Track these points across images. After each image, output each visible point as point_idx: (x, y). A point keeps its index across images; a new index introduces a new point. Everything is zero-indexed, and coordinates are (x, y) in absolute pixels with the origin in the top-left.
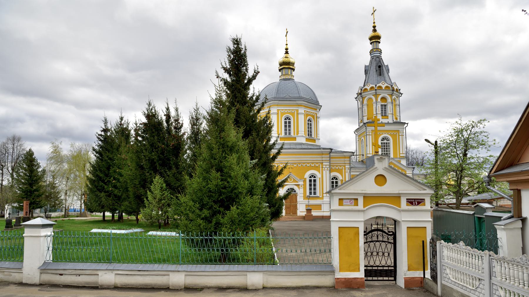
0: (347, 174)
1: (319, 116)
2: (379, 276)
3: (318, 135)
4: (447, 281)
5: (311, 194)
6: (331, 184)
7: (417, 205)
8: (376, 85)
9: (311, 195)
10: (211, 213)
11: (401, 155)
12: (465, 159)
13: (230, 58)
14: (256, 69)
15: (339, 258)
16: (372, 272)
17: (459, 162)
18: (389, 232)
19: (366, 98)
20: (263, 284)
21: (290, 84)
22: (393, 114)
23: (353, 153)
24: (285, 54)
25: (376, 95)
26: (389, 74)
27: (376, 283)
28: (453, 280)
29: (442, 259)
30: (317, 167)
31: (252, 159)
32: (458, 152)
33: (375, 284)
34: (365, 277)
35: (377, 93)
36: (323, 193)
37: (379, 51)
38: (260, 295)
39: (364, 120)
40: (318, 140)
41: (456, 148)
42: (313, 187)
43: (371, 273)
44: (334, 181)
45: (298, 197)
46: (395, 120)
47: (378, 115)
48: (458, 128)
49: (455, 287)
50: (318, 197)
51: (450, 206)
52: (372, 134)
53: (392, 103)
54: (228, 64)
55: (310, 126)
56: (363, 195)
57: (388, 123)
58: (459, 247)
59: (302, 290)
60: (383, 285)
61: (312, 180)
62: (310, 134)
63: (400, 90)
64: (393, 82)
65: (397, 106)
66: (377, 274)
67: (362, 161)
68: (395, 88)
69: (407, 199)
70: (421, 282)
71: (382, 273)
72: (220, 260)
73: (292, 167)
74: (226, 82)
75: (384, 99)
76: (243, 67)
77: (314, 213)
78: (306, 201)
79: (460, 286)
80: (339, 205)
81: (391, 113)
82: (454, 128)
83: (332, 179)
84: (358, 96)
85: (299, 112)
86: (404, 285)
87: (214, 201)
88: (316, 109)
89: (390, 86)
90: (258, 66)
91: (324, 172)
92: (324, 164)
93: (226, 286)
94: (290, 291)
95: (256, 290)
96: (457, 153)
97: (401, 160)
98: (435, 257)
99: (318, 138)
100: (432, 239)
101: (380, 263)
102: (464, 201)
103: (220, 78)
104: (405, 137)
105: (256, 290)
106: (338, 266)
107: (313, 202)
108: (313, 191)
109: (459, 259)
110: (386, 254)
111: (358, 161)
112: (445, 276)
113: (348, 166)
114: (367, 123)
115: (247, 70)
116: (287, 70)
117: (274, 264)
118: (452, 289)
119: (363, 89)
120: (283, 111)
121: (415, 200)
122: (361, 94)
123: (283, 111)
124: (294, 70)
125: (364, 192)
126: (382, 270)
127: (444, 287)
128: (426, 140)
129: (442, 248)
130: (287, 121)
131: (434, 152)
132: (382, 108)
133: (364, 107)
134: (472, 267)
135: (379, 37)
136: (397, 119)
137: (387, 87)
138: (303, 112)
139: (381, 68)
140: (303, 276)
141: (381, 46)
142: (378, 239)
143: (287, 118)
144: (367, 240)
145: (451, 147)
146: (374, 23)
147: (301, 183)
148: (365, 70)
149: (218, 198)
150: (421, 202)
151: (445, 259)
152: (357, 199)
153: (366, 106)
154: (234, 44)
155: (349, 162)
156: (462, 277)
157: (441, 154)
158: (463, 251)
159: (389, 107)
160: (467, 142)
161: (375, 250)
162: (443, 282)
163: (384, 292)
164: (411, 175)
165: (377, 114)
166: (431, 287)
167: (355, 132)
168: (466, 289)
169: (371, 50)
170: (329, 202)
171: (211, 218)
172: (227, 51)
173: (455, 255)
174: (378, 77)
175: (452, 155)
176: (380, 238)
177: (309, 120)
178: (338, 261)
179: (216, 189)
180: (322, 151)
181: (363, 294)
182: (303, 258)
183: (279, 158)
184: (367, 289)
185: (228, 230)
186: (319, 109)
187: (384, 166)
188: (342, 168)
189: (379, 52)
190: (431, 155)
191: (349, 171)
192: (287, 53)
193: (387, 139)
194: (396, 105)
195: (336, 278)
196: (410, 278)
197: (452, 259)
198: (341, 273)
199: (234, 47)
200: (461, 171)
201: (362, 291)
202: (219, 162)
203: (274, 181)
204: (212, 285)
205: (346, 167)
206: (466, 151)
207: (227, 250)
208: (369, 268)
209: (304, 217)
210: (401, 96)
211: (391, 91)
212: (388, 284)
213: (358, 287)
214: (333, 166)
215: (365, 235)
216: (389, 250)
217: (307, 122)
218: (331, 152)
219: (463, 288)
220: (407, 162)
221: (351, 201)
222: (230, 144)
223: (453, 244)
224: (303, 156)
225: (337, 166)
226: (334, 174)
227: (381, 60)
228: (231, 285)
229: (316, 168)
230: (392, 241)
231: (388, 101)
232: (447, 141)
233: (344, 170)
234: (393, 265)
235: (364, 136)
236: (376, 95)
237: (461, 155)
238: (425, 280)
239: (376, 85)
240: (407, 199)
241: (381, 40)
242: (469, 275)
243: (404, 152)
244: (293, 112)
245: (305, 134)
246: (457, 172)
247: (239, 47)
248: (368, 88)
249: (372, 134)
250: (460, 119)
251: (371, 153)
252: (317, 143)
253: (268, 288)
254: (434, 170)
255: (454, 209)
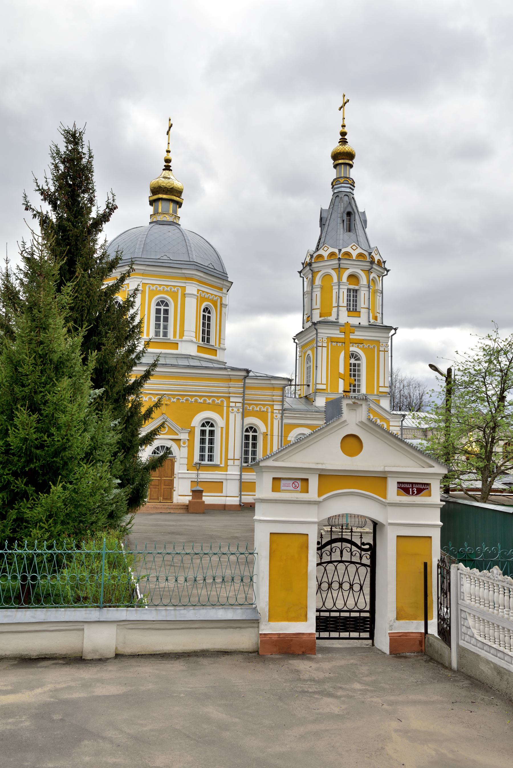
0: (276, 422)
1: (227, 303)
2: (341, 629)
3: (222, 341)
4: (469, 641)
5: (202, 460)
6: (244, 441)
7: (416, 495)
8: (340, 250)
9: (203, 462)
10: (5, 497)
11: (381, 389)
12: (501, 408)
13: (58, 170)
14: (111, 201)
15: (268, 595)
16: (328, 621)
17: (491, 411)
18: (363, 544)
19: (320, 274)
20: (116, 648)
21: (170, 234)
22: (369, 309)
23: (291, 380)
24: (164, 170)
25: (339, 269)
26: (367, 230)
27: (336, 644)
28: (480, 639)
29: (461, 599)
30: (218, 405)
31: (97, 386)
32: (488, 393)
33: (334, 646)
34: (316, 632)
35: (342, 266)
36: (227, 459)
37: (350, 182)
38: (110, 671)
39: (314, 316)
40: (221, 350)
41: (485, 385)
42: (207, 445)
43: (328, 624)
44: (251, 434)
45: (176, 465)
46: (372, 321)
47: (340, 308)
48: (492, 346)
49: (483, 653)
50: (217, 467)
51: (470, 493)
52: (328, 345)
53: (369, 287)
54: (51, 182)
55: (206, 322)
56: (319, 473)
57: (359, 327)
58: (491, 577)
59: (195, 659)
60: (349, 648)
61: (205, 430)
62: (206, 336)
63: (384, 262)
64: (372, 246)
65: (378, 294)
66: (338, 626)
67: (306, 396)
68: (377, 258)
69: (398, 483)
70: (421, 643)
71: (348, 624)
72: (18, 598)
73: (168, 403)
74: (44, 221)
75: (353, 277)
76: (84, 192)
77: (208, 499)
78: (193, 474)
79: (492, 651)
80: (273, 491)
81: (366, 306)
82: (484, 346)
83: (247, 431)
84: (304, 268)
85: (187, 292)
86: (389, 647)
87: (15, 474)
88: (221, 289)
89: (366, 254)
90: (114, 195)
91: (232, 416)
92: (232, 399)
93: (38, 653)
94: (172, 662)
95: (100, 660)
96: (486, 394)
97: (381, 398)
98: (446, 594)
99: (222, 346)
100: (442, 560)
101: (345, 604)
102: (497, 485)
103: (33, 210)
104: (390, 355)
105: (101, 661)
106: (267, 609)
107: (206, 475)
108: (207, 454)
109: (490, 599)
110: (357, 588)
111: (297, 396)
112: (466, 632)
113: (277, 407)
114: (319, 322)
115: (91, 200)
116: (166, 204)
117: (140, 607)
118: (478, 656)
119: (315, 255)
120: (154, 288)
121: (412, 486)
122: (310, 264)
123: (154, 288)
124: (180, 204)
125: (320, 467)
126: (346, 618)
127: (462, 652)
128: (431, 366)
129: (461, 578)
130: (162, 308)
131: (445, 390)
132: (349, 296)
133: (314, 290)
134: (474, 600)
135: (351, 156)
136: (376, 318)
137: (360, 255)
138: (196, 293)
139: (352, 217)
140: (197, 630)
141: (353, 173)
142: (341, 557)
143: (162, 302)
144: (321, 559)
145: (476, 383)
146: (344, 126)
147: (184, 436)
148: (321, 219)
149: (24, 467)
150: (424, 489)
151: (466, 598)
152: (307, 480)
153: (319, 289)
154: (68, 142)
155: (280, 398)
156: (491, 631)
157: (457, 394)
158: (498, 585)
159: (363, 294)
160: (506, 374)
161: (336, 578)
162: (462, 643)
163: (352, 661)
164: (395, 430)
165: (338, 306)
166: (439, 653)
167: (294, 339)
168: (503, 657)
169: (334, 180)
170: (238, 477)
171: (4, 508)
172: (52, 156)
173: (483, 592)
174: (345, 235)
175: (479, 398)
176: (346, 557)
177: (206, 310)
178: (268, 600)
179: (24, 447)
180: (229, 373)
181: (314, 665)
182: (190, 592)
183: (148, 386)
184: (320, 656)
185: (44, 533)
186: (228, 288)
187: (359, 419)
188: (267, 409)
189: (349, 185)
190: (440, 397)
191: (279, 416)
192: (167, 168)
193: (356, 356)
194: (375, 292)
195: (261, 634)
196: (401, 634)
197: (479, 599)
198: (271, 623)
199: (68, 150)
200: (494, 429)
201: (310, 659)
202: (31, 392)
203: (134, 433)
204: (8, 653)
205: (276, 407)
206: (503, 390)
207: (34, 578)
208: (322, 614)
209: (187, 506)
210: (387, 275)
211: (368, 264)
212: (359, 646)
213: (303, 652)
214: (250, 405)
215: (318, 549)
216: (362, 579)
217: (202, 313)
218: (248, 376)
219: (485, 648)
220: (391, 403)
221: (296, 483)
222: (55, 357)
223: (480, 571)
224: (190, 382)
225: (257, 405)
226: (250, 420)
227: (352, 200)
228: (48, 652)
229: (217, 408)
230: (368, 562)
231: (361, 283)
232: (470, 370)
233: (269, 414)
234: (368, 608)
235: (312, 349)
236: (339, 269)
237: (494, 398)
238: (428, 639)
239: (340, 250)
240: (399, 483)
241: (355, 162)
242: (493, 624)
243: (387, 384)
244: (174, 292)
245: (196, 337)
246: (486, 429)
247: (77, 150)
248: (325, 254)
249: (328, 345)
250: (495, 330)
251: (324, 381)
252: (220, 356)
253: (126, 655)
254: (442, 425)
255: (478, 501)
